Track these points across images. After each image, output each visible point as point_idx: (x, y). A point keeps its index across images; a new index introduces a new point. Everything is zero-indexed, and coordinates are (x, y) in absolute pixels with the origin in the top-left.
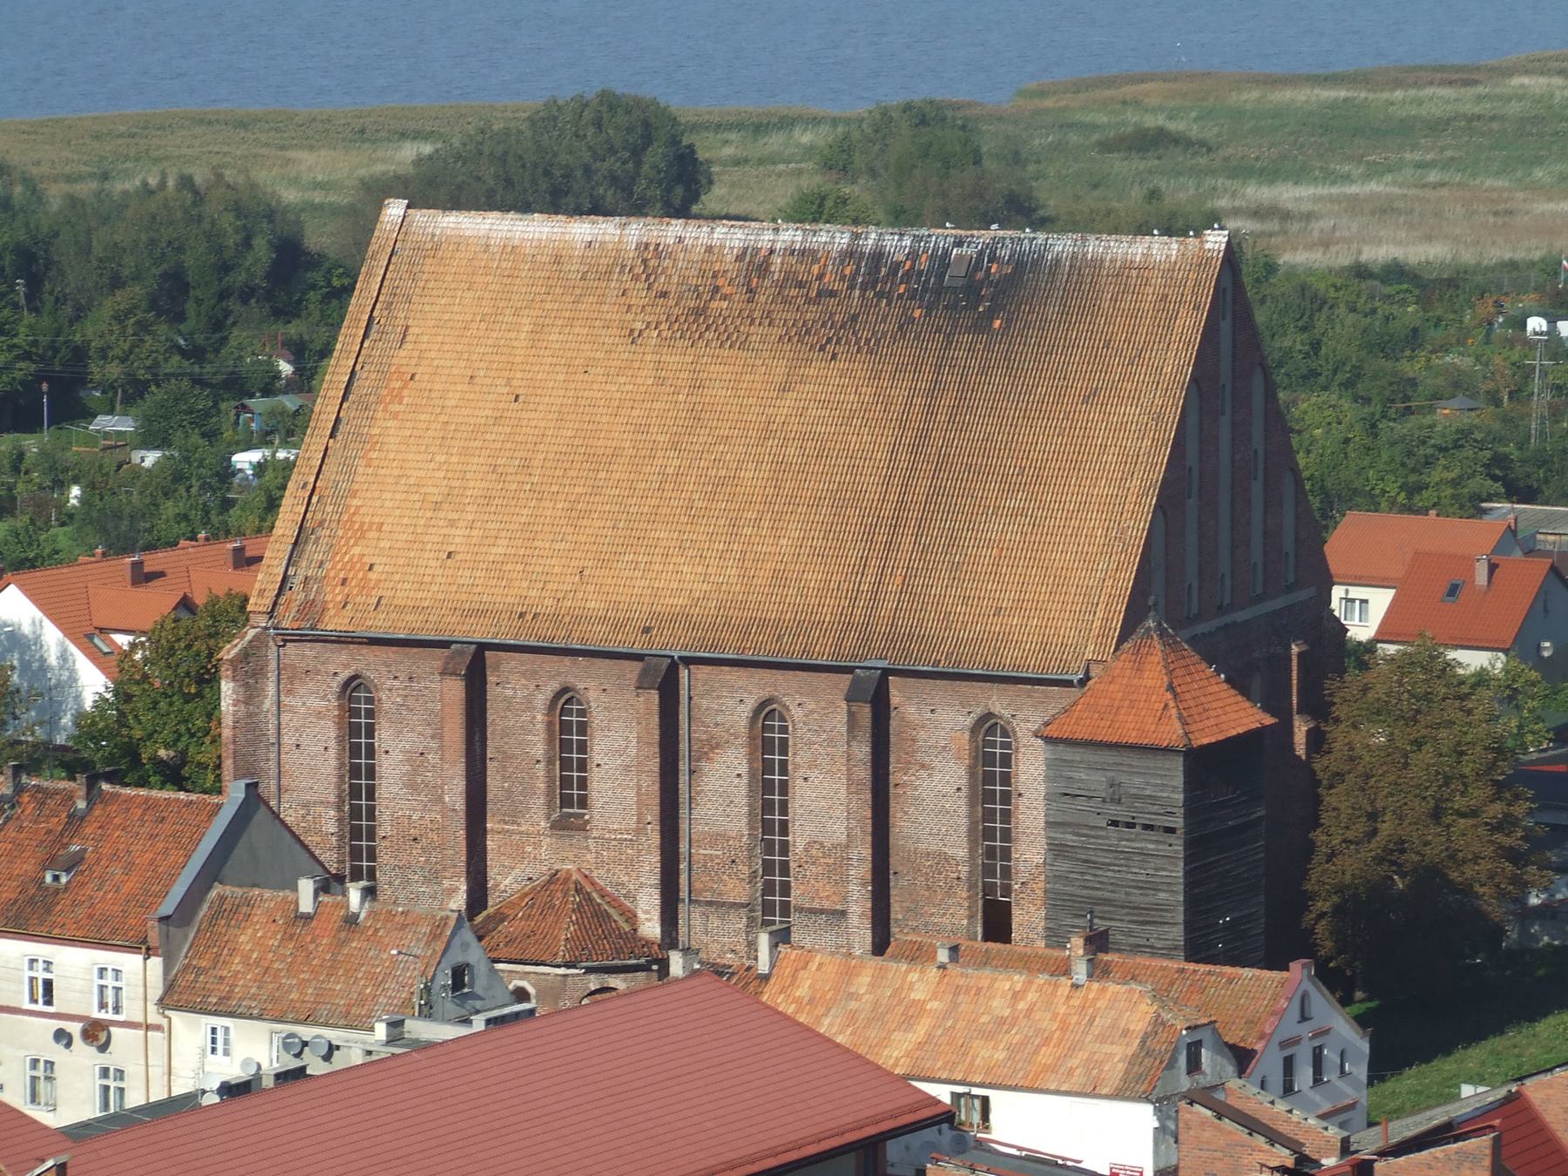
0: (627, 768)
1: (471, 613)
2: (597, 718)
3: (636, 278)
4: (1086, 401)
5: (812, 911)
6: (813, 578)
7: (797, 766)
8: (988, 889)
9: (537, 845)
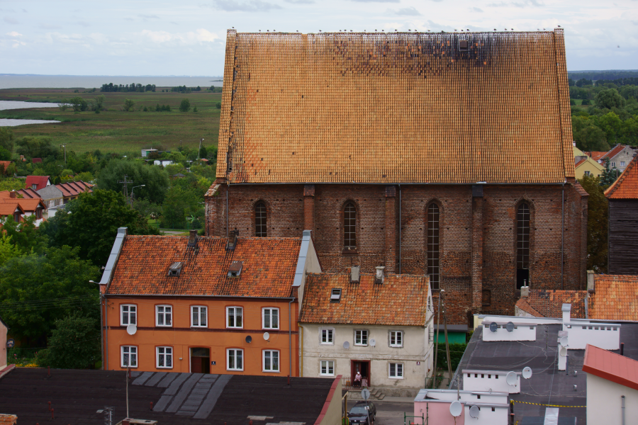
0: (374, 229)
1: (310, 173)
2: (362, 210)
3: (337, 53)
4: (530, 87)
5: (450, 278)
6: (444, 154)
7: (444, 224)
8: (519, 265)
9: (337, 260)
